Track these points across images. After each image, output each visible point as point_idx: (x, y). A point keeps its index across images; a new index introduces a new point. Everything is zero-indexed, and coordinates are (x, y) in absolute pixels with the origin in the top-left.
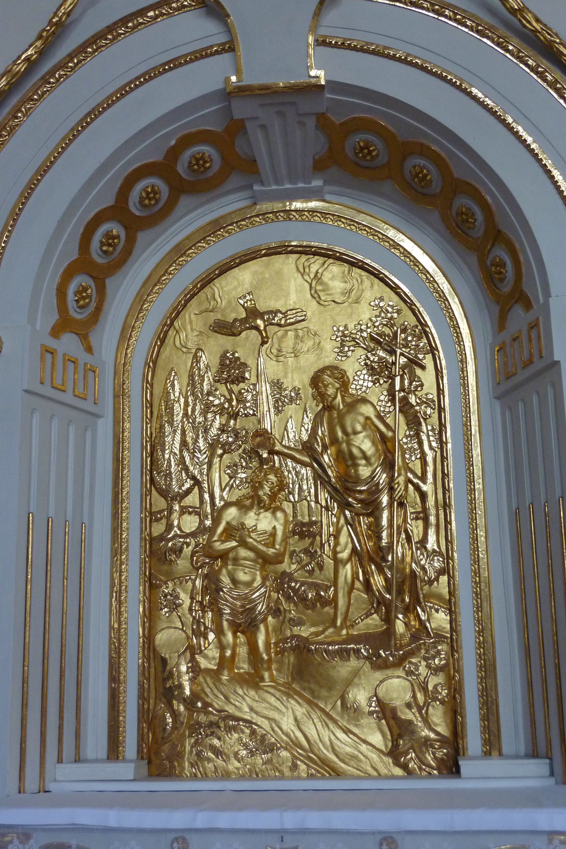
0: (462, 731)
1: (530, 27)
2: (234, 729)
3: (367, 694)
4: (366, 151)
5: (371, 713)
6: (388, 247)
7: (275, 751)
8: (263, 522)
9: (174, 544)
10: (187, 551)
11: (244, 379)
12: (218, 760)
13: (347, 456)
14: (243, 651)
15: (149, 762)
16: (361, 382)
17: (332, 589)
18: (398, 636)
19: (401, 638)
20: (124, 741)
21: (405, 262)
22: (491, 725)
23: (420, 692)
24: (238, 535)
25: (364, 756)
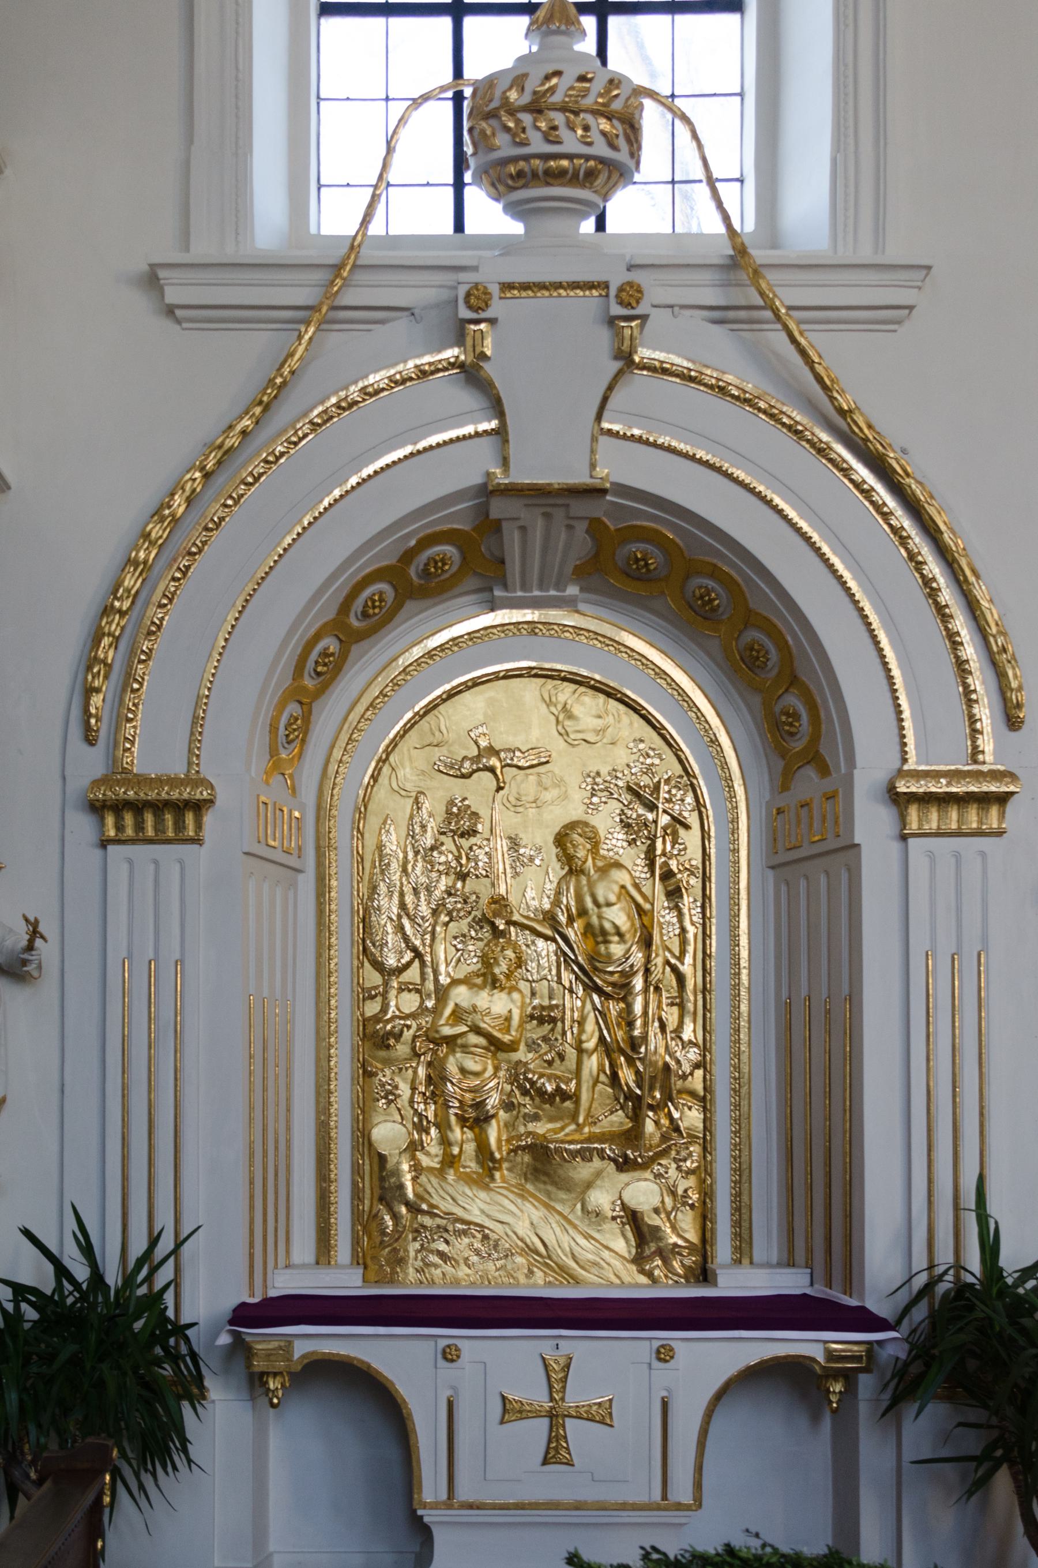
1: (861, 435)
2: (465, 1233)
5: (614, 1218)
8: (497, 1005)
10: (408, 1035)
11: (474, 832)
13: (597, 931)
14: (470, 1148)
15: (366, 1268)
16: (616, 843)
17: (574, 1082)
18: (647, 1136)
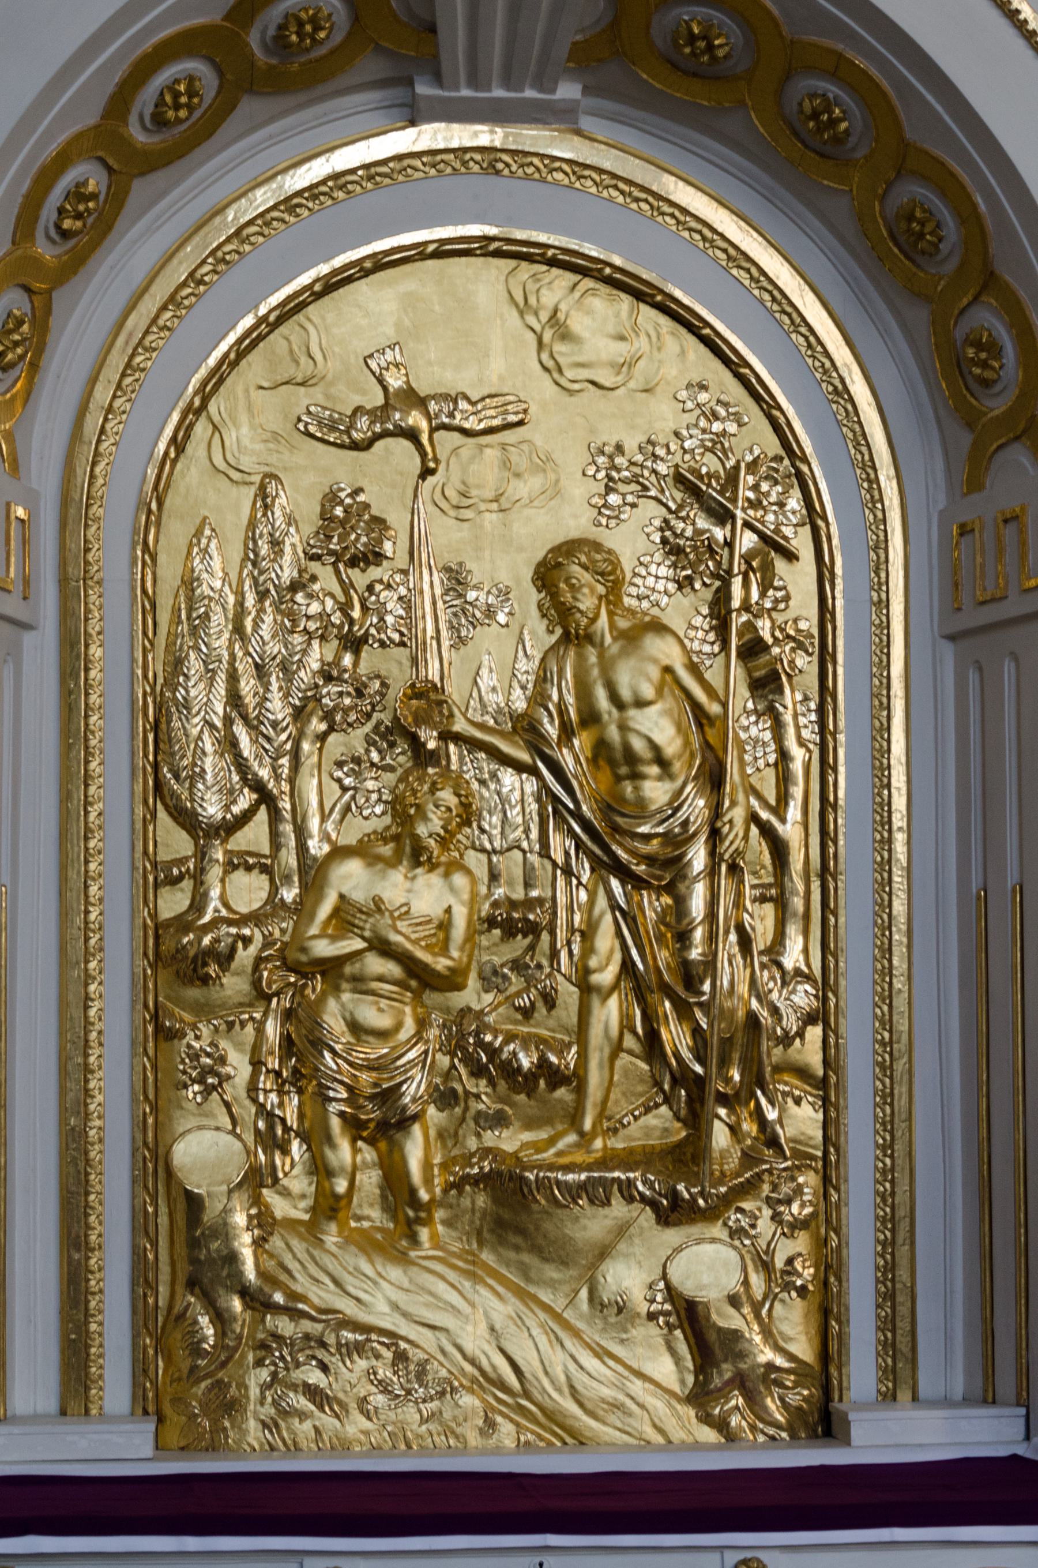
0: (839, 1352)
2: (359, 1348)
3: (644, 1276)
4: (702, 44)
5: (652, 1316)
6: (724, 263)
7: (448, 1396)
8: (423, 897)
9: (217, 940)
10: (245, 956)
12: (322, 1415)
14: (370, 1180)
15: (161, 1420)
16: (652, 584)
17: (574, 1049)
18: (716, 1155)
19: (722, 1158)
20: (101, 1376)
21: (762, 302)
22: (898, 1338)
23: (757, 1271)
24: (368, 926)
25: (638, 1404)
